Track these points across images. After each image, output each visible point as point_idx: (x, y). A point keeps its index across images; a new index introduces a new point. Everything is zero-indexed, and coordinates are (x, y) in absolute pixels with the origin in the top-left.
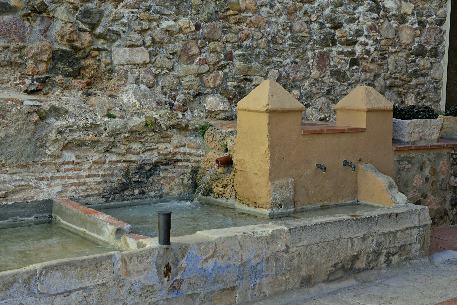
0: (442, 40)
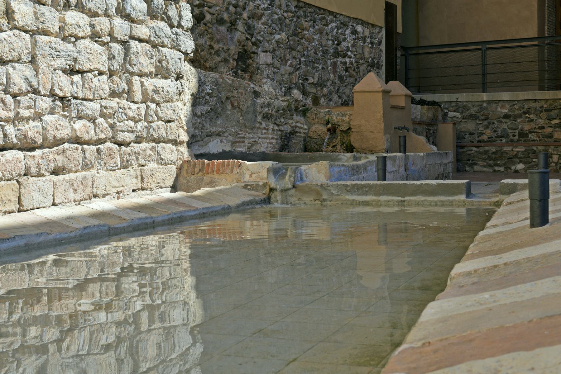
0: (380, 57)
